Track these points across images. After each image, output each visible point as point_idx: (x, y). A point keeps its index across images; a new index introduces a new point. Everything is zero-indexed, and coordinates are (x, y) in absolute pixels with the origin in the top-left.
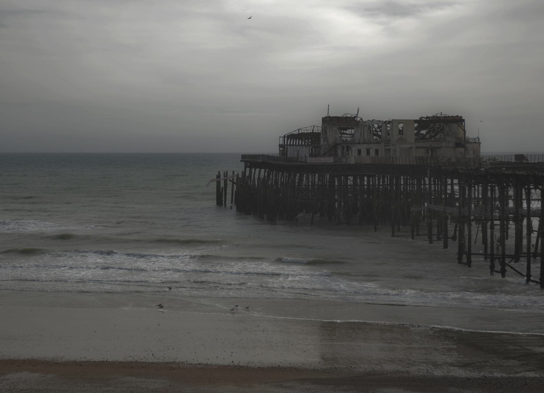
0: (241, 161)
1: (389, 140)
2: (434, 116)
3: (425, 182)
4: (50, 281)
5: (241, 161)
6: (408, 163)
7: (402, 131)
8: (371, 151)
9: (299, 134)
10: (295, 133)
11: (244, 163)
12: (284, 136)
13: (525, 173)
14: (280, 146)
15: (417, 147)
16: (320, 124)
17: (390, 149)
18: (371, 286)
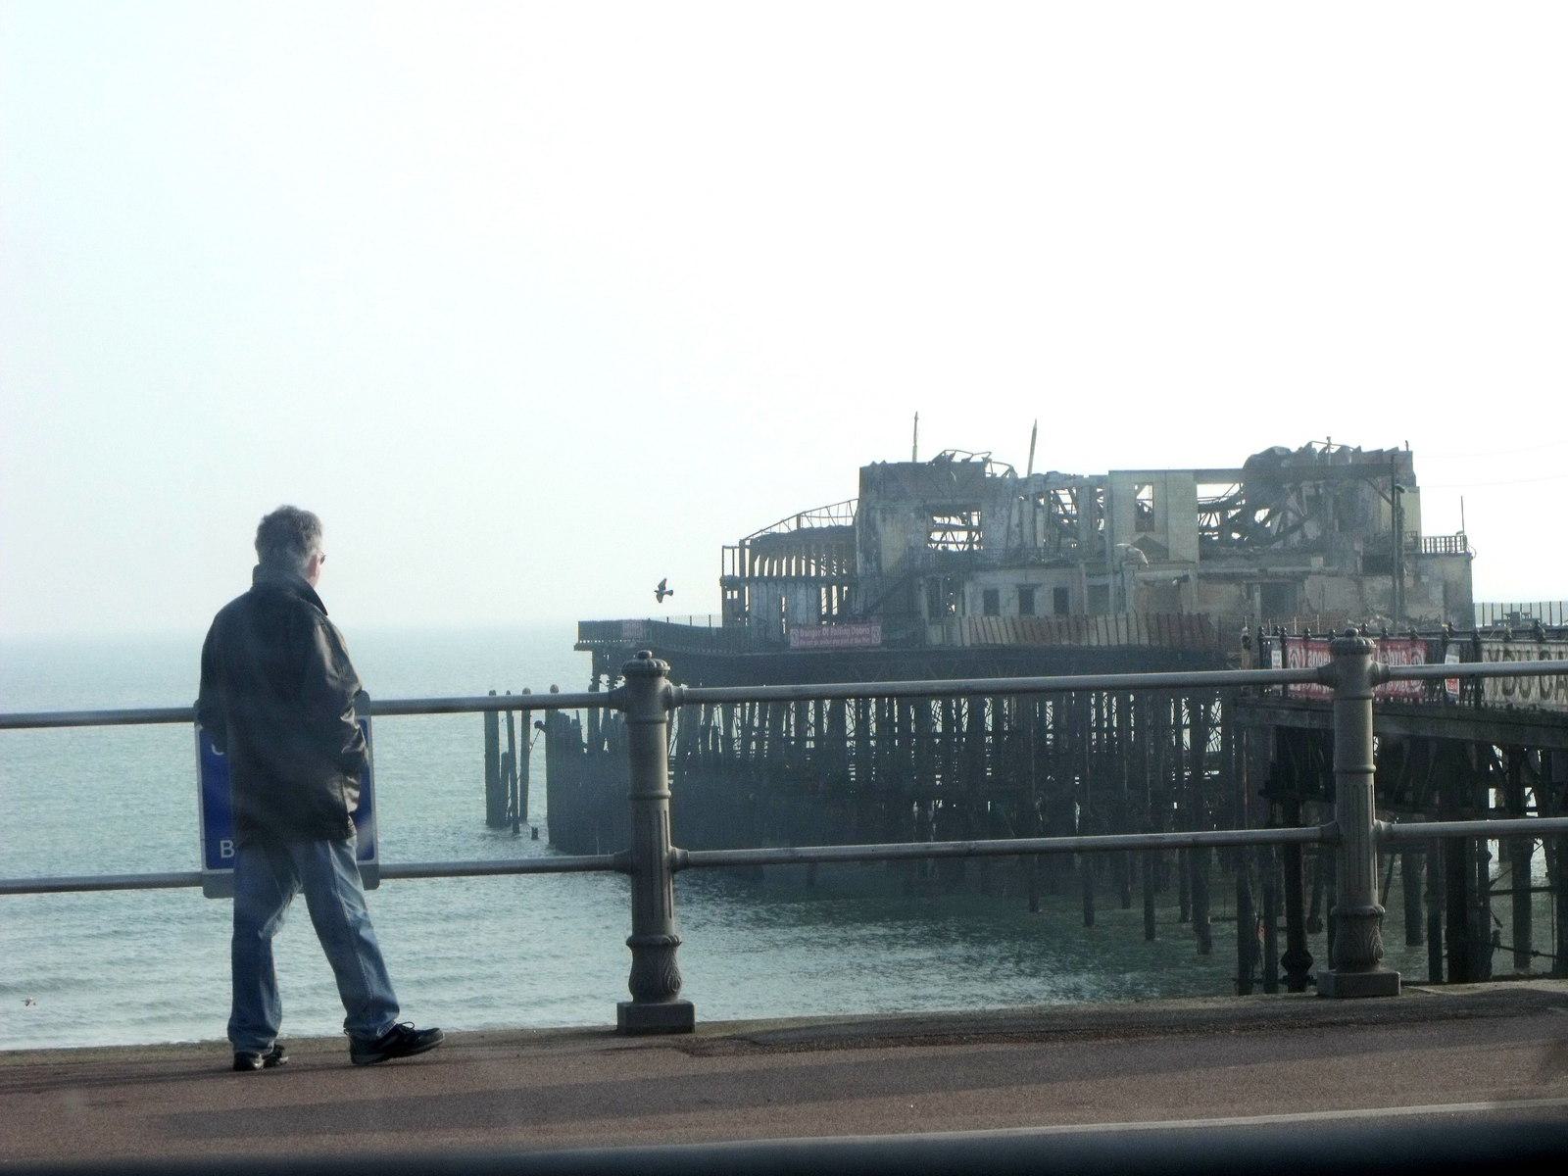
0: (578, 647)
1: (1102, 553)
2: (1307, 451)
3: (760, 746)
4: (651, 1047)
5: (578, 647)
6: (1123, 641)
7: (1150, 516)
8: (1038, 595)
9: (800, 531)
10: (784, 529)
11: (589, 654)
12: (742, 545)
13: (1559, 633)
14: (727, 583)
15: (1206, 577)
16: (853, 490)
17: (1107, 587)
18: (1187, 941)
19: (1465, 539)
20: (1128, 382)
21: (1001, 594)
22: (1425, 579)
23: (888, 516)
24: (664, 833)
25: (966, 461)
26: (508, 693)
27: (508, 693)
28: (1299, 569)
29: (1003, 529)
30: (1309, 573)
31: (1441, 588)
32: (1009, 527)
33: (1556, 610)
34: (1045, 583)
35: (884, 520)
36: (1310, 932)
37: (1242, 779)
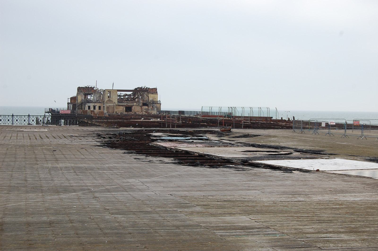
8: (96, 107)
14: (68, 103)
19: (160, 101)
20: (116, 77)
21: (91, 107)
22: (154, 107)
23: (79, 95)
24: (129, 129)
25: (91, 87)
26: (282, 118)
27: (282, 118)
28: (132, 105)
29: (96, 97)
30: (134, 105)
31: (156, 108)
32: (97, 97)
33: (207, 113)
34: (97, 105)
35: (78, 95)
36: (321, 126)
37: (272, 123)
